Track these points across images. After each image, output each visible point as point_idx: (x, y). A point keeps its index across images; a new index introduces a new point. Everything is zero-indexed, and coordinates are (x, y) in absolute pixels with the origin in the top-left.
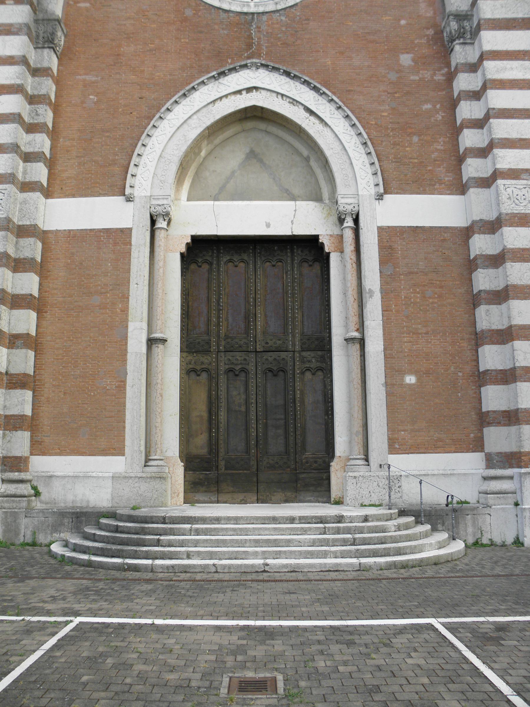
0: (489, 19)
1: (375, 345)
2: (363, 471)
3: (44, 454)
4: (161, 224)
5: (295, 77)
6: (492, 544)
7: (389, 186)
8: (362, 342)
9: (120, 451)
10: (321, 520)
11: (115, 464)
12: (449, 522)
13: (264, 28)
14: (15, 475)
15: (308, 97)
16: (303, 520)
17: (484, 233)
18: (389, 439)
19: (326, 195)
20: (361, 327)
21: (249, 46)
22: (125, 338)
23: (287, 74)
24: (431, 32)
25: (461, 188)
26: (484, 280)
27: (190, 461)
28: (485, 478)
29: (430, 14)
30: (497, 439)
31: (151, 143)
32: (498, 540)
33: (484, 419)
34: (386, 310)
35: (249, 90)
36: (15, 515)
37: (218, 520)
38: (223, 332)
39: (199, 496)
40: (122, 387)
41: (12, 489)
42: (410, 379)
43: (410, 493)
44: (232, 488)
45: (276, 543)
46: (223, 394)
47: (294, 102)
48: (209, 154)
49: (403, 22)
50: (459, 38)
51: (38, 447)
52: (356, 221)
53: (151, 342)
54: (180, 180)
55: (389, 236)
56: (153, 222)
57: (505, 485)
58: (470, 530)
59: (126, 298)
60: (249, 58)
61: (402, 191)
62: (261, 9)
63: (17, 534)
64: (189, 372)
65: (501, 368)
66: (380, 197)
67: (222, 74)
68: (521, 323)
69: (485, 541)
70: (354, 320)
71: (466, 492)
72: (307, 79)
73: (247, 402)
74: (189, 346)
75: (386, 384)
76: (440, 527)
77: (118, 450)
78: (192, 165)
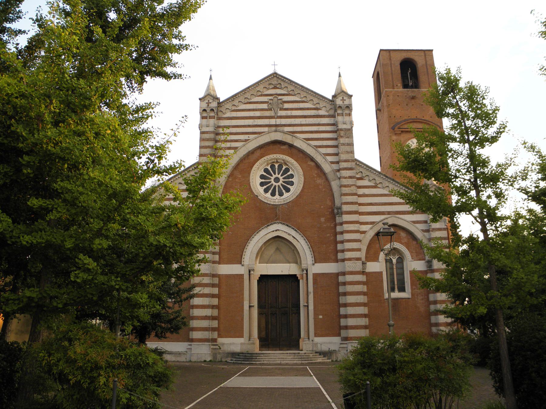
1: (311, 307)
2: (307, 342)
3: (221, 337)
4: (252, 272)
5: (290, 227)
7: (316, 260)
8: (308, 306)
9: (242, 337)
10: (294, 354)
11: (241, 340)
12: (329, 355)
13: (280, 209)
14: (215, 343)
15: (293, 233)
16: (290, 353)
19: (299, 262)
20: (307, 302)
21: (276, 216)
22: (243, 306)
23: (287, 226)
24: (330, 210)
25: (337, 261)
26: (341, 289)
27: (260, 338)
28: (341, 344)
29: (330, 204)
31: (248, 248)
33: (341, 328)
34: (314, 297)
35: (276, 230)
36: (216, 354)
37: (270, 354)
38: (270, 302)
39: (263, 349)
40: (242, 319)
41: (215, 347)
42: (321, 317)
43: (320, 348)
44: (125, 246)
45: (283, 358)
46: (270, 321)
47: (289, 234)
48: (265, 249)
51: (220, 336)
52: (307, 271)
53: (250, 307)
54: (256, 258)
55: (316, 276)
56: (250, 272)
57: (345, 346)
59: (243, 294)
60: (276, 220)
61: (320, 262)
62: (280, 203)
63: (216, 359)
64: (260, 314)
66: (313, 264)
67: (269, 226)
70: (306, 300)
71: (333, 348)
73: (263, 364)
74: (260, 306)
75: (314, 318)
77: (242, 336)
78: (261, 255)
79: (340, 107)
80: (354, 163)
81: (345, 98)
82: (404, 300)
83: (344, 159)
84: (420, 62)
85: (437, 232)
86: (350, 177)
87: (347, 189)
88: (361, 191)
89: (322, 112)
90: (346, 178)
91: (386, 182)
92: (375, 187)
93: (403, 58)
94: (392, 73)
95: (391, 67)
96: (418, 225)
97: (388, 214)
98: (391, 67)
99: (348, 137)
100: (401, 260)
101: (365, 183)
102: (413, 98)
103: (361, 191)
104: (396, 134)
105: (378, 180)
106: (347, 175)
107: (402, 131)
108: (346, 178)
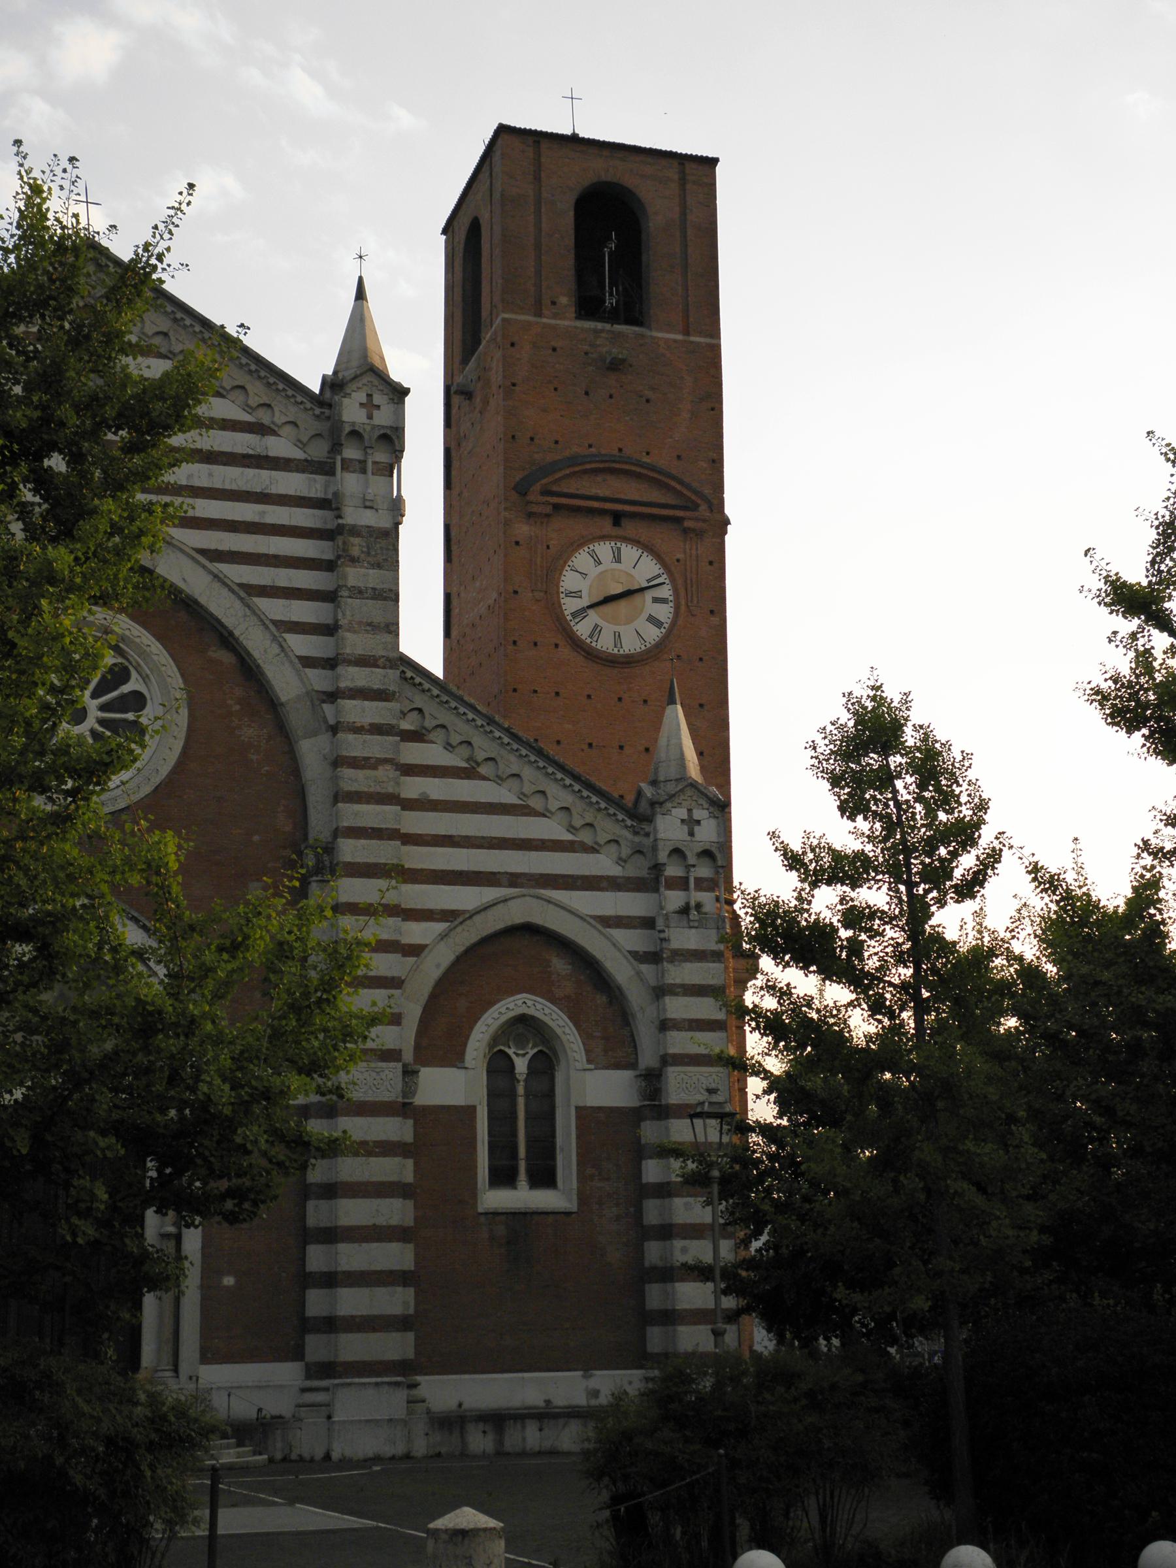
0: (349, 863)
6: (301, 1459)
17: (321, 1117)
18: (202, 1348)
30: (317, 1347)
32: (306, 1456)
33: (306, 1325)
42: (229, 1281)
49: (256, 838)
50: (316, 874)
57: (320, 1397)
58: (279, 1445)
65: (326, 1270)
68: (346, 1224)
69: (294, 1456)
71: (278, 1405)
72: (136, 914)
76: (247, 1442)
79: (355, 434)
80: (393, 674)
81: (378, 399)
82: (550, 1219)
83: (359, 651)
84: (659, 205)
85: (688, 966)
86: (378, 729)
87: (361, 774)
88: (413, 787)
89: (279, 447)
90: (358, 730)
91: (512, 758)
92: (468, 773)
93: (587, 180)
94: (538, 246)
95: (538, 212)
96: (618, 934)
97: (512, 885)
98: (538, 212)
99: (379, 566)
100: (546, 1064)
101: (431, 753)
102: (615, 366)
103: (413, 787)
104: (530, 515)
105: (484, 747)
106: (366, 720)
107: (557, 507)
108: (358, 730)
